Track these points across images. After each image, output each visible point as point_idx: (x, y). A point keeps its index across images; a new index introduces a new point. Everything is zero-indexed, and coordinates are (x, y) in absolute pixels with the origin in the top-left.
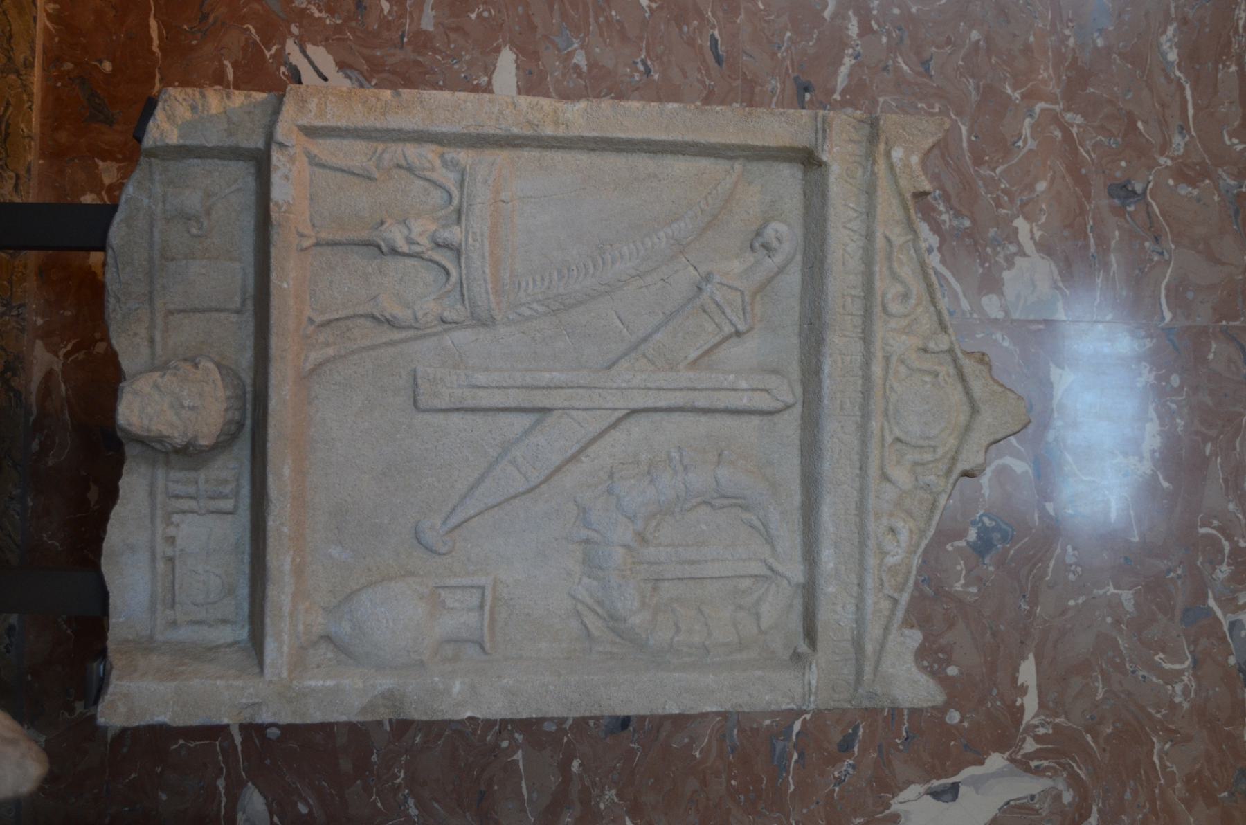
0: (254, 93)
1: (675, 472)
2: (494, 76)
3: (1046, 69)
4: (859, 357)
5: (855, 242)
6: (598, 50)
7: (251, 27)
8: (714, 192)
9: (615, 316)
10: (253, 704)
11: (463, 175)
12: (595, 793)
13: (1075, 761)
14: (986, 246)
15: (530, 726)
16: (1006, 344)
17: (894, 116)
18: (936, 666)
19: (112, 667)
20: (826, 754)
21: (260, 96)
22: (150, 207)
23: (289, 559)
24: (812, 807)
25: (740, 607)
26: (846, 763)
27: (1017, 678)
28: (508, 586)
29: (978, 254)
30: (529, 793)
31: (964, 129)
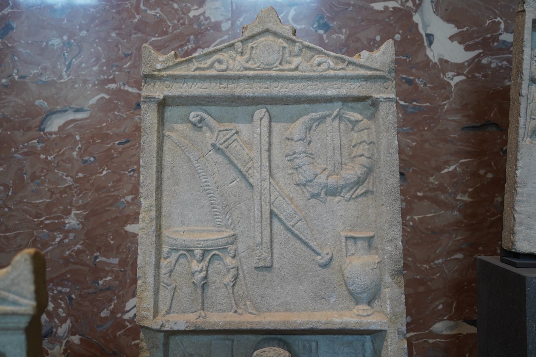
0: (141, 338)
3: (126, 4)
6: (125, 191)
7: (119, 333)
8: (178, 144)
9: (231, 184)
11: (173, 249)
12: (431, 186)
14: (201, 29)
15: (404, 213)
16: (241, 20)
18: (376, 45)
26: (417, 82)
28: (345, 227)
29: (204, 33)
30: (431, 213)
31: (153, 39)
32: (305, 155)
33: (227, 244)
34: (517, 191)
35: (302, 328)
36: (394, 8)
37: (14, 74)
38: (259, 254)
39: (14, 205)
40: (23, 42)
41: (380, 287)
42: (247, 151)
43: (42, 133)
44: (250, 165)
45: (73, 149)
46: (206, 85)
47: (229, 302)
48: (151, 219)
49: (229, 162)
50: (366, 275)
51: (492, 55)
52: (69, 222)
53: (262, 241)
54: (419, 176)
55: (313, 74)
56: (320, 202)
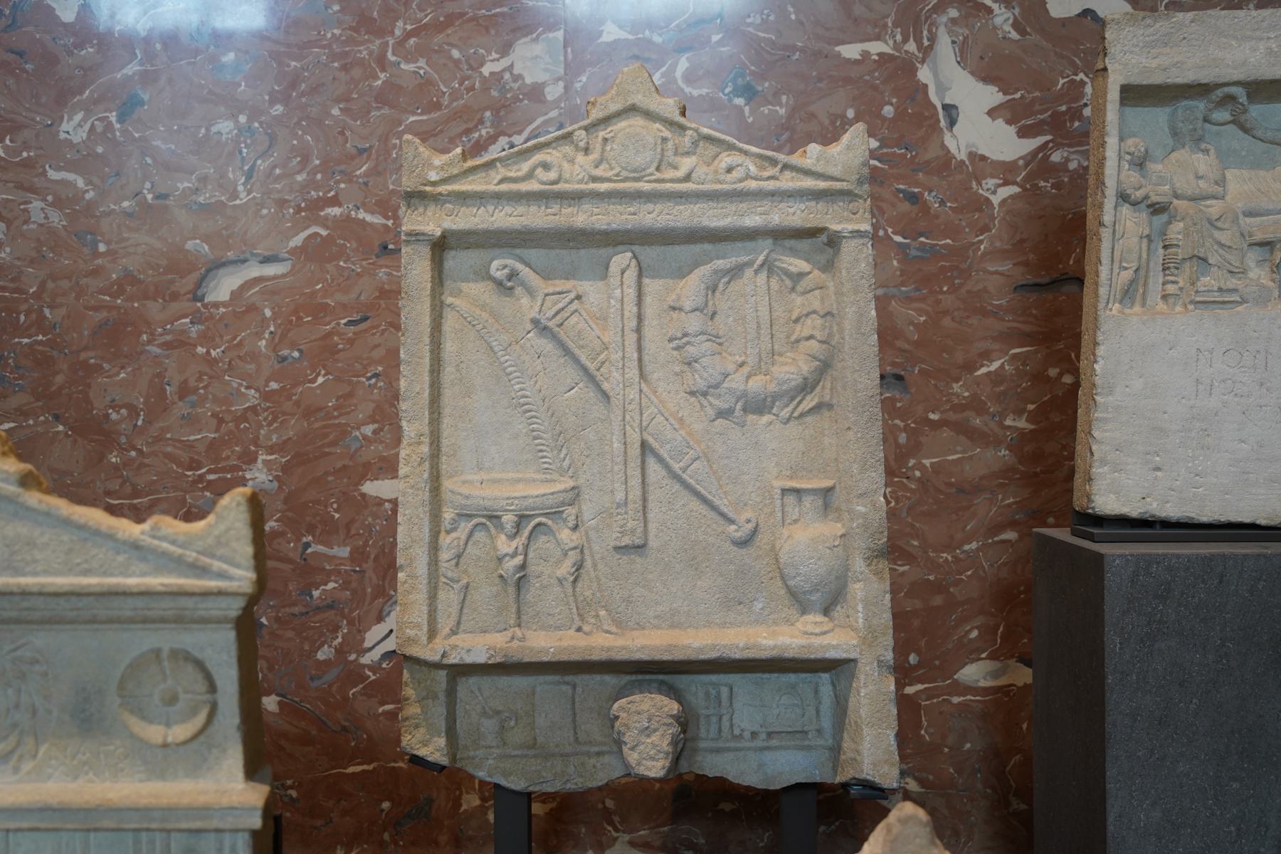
0: (404, 680)
2: (384, 497)
3: (360, 52)
6: (361, 416)
7: (351, 692)
8: (469, 319)
9: (568, 394)
11: (462, 515)
12: (956, 401)
13: (924, 8)
16: (584, 79)
17: (404, 179)
19: (855, 778)
21: (406, 675)
24: (964, 224)
27: (856, 60)
31: (412, 119)
32: (704, 338)
33: (563, 504)
34: (1095, 402)
35: (702, 657)
37: (145, 192)
38: (621, 523)
39: (148, 444)
40: (162, 129)
41: (846, 582)
42: (598, 332)
43: (199, 304)
44: (602, 357)
45: (259, 335)
46: (521, 209)
47: (567, 611)
48: (422, 458)
49: (564, 353)
50: (819, 559)
51: (1070, 146)
52: (253, 477)
53: (626, 498)
55: (718, 187)
56: (733, 426)
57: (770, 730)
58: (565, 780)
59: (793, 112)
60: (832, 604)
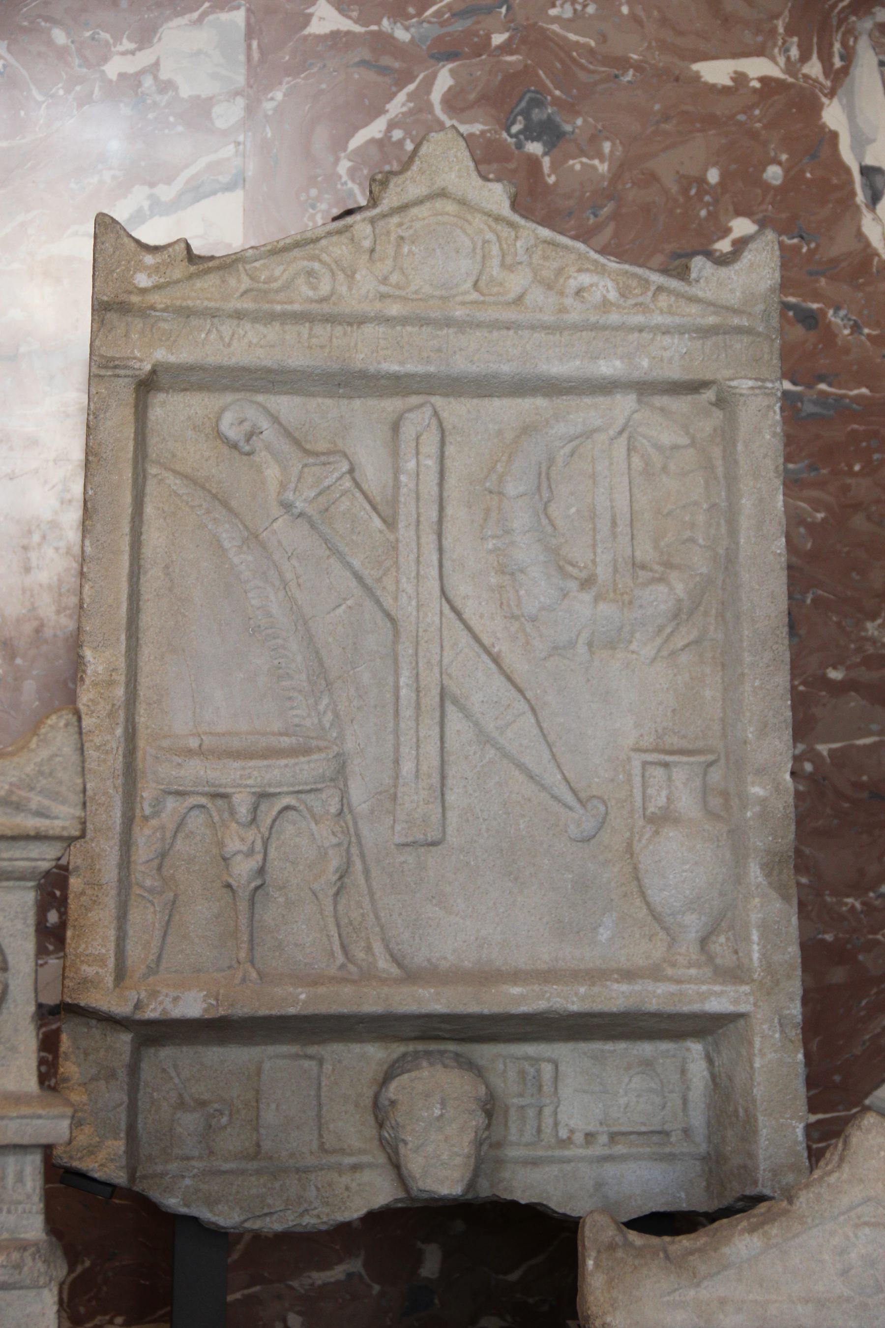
1: (512, 543)
4: (381, 330)
5: (246, 332)
8: (185, 497)
9: (332, 614)
10: (781, 1025)
12: (871, 650)
13: (835, 5)
18: (707, 198)
20: (820, 346)
22: (194, 1176)
23: (615, 986)
25: (664, 468)
26: (833, 319)
28: (642, 735)
30: (870, 733)
36: (765, 80)
54: (835, 619)
57: (614, 1129)
58: (301, 1210)
59: (620, 170)
60: (711, 933)
